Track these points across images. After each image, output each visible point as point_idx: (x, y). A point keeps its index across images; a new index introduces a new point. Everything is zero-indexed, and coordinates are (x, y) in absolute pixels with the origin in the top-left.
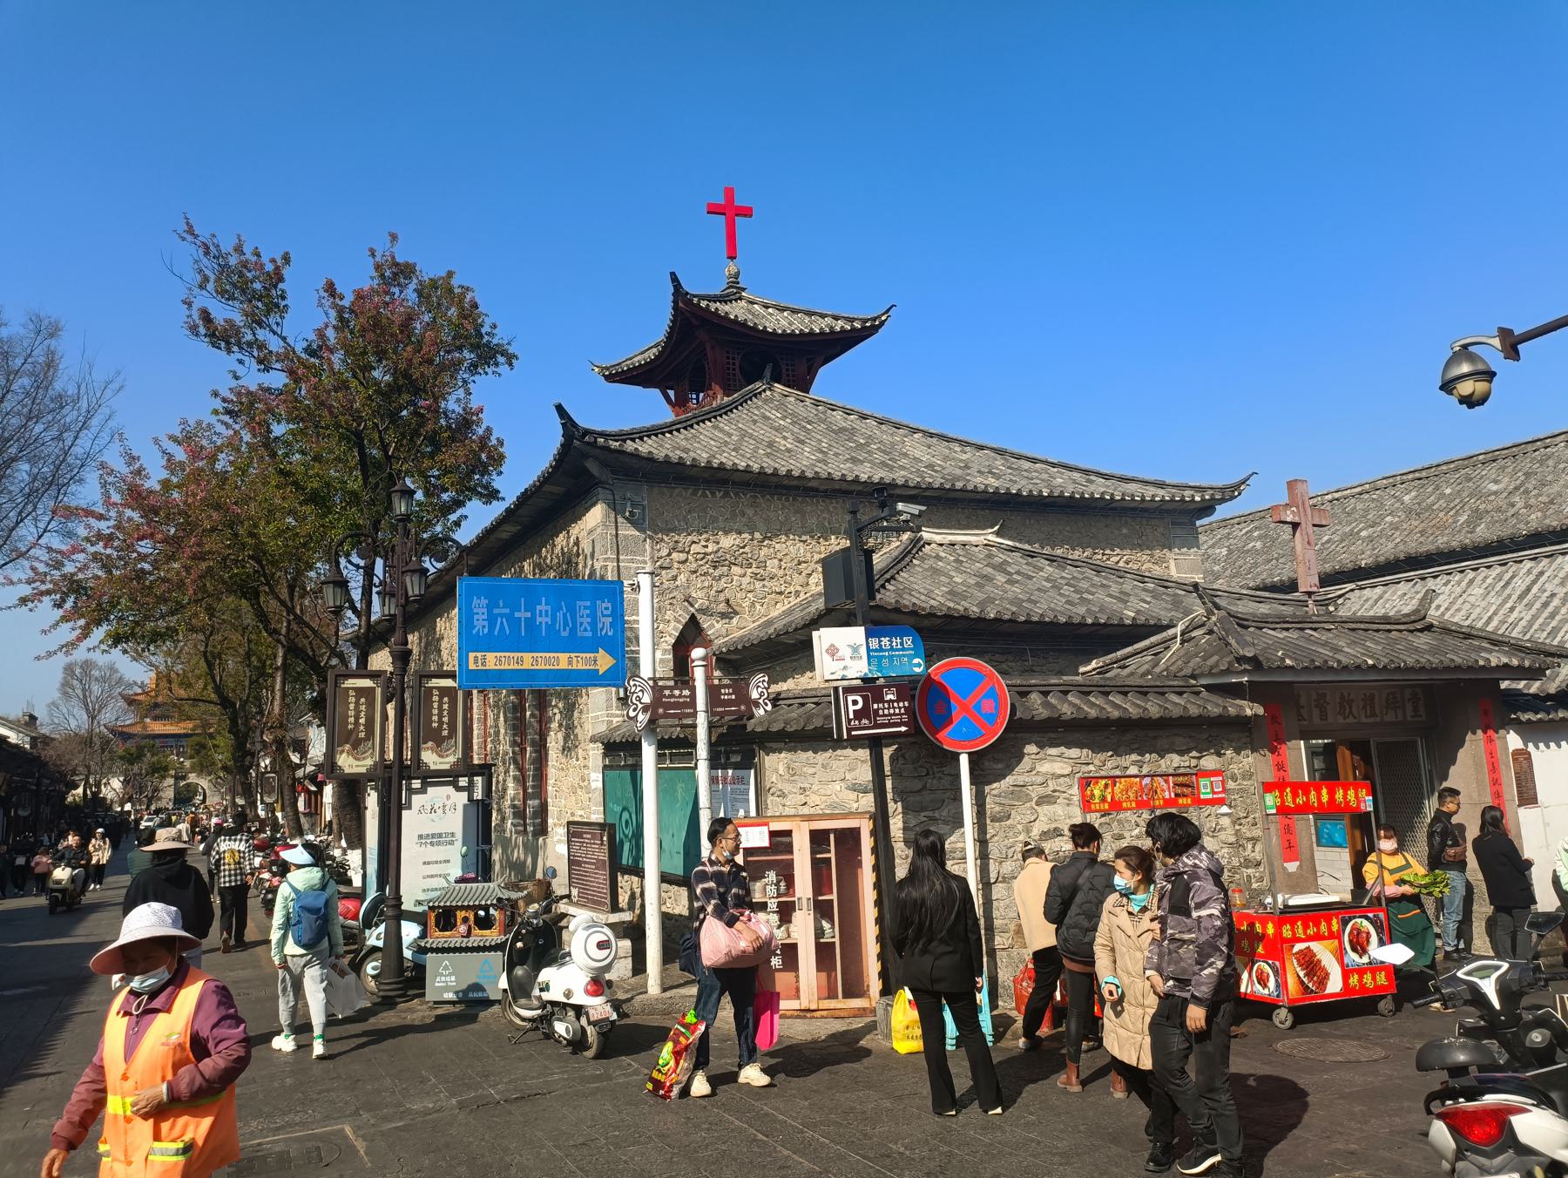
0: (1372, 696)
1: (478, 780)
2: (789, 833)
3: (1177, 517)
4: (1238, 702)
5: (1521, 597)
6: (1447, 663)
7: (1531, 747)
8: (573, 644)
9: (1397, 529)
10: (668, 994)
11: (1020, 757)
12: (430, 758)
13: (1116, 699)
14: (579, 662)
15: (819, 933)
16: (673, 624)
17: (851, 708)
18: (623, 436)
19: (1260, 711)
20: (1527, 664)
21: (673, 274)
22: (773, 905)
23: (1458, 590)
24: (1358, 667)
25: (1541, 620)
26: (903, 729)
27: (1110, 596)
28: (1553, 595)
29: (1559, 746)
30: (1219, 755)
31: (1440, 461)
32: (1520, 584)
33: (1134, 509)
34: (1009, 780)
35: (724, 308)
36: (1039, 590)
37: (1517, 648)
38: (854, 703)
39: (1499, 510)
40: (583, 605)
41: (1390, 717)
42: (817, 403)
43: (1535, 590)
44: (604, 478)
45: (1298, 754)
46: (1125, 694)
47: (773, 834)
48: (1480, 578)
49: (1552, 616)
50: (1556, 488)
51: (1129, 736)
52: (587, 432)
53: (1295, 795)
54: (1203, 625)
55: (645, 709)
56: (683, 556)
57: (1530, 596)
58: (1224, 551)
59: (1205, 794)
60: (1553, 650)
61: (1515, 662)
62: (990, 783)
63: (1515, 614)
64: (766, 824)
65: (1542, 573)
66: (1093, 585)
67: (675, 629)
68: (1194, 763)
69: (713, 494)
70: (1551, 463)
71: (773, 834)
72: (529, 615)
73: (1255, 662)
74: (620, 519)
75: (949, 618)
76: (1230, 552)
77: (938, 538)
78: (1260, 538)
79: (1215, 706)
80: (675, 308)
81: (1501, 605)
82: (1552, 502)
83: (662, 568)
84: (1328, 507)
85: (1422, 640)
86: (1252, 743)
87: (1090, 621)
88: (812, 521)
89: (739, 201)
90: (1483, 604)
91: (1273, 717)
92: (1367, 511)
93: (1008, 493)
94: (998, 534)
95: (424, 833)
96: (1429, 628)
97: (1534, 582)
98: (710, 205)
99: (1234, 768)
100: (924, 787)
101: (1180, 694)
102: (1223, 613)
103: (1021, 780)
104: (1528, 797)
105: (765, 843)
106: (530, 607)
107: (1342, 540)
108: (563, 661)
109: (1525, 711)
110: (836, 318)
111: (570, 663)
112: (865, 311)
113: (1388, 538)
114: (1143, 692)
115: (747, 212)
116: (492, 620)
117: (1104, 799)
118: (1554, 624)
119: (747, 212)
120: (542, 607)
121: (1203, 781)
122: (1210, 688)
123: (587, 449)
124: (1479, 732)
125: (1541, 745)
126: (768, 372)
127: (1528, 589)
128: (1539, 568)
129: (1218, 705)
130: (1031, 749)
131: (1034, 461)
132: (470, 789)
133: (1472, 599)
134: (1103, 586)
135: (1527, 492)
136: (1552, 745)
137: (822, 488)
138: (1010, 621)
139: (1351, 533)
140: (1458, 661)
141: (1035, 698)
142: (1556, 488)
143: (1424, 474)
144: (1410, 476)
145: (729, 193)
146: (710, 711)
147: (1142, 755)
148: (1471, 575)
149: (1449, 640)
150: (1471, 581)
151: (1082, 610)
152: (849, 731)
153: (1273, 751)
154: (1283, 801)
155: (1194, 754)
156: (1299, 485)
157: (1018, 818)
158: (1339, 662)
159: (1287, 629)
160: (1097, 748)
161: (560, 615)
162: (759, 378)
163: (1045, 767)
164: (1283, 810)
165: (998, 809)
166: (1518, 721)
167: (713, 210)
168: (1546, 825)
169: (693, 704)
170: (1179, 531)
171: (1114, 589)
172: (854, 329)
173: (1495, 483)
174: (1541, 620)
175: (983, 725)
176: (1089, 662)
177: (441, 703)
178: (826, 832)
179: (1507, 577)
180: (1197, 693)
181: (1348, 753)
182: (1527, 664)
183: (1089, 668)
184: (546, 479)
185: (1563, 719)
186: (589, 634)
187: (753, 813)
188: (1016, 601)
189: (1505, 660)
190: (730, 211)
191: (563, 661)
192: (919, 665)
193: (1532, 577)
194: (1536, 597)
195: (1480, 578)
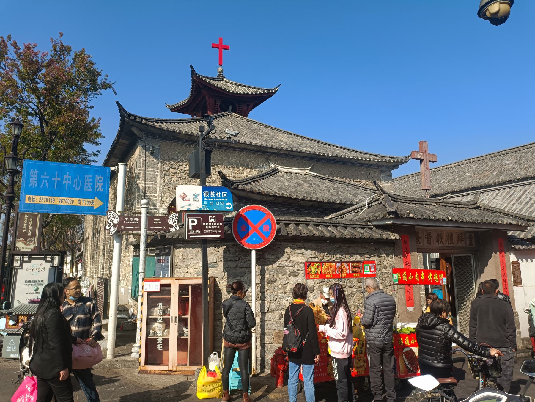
0: (452, 235)
1: (57, 258)
2: (169, 285)
3: (385, 168)
4: (389, 233)
5: (517, 200)
6: (484, 221)
7: (520, 261)
8: (81, 194)
9: (470, 177)
10: (115, 359)
11: (283, 253)
12: (21, 246)
13: (331, 229)
14: (85, 202)
15: (181, 333)
16: (168, 198)
17: (191, 224)
18: (152, 120)
19: (398, 237)
20: (519, 224)
21: (191, 65)
22: (160, 319)
23: (492, 197)
24: (444, 220)
25: (525, 209)
26: (218, 236)
27: (350, 194)
28: (531, 199)
29: (532, 261)
30: (379, 257)
31: (488, 154)
32: (517, 195)
33: (367, 164)
34: (277, 264)
35: (216, 83)
36: (320, 190)
37: (516, 217)
38: (193, 222)
39: (509, 170)
40: (88, 178)
41: (459, 245)
42: (248, 121)
43: (523, 197)
44: (141, 136)
45: (417, 259)
46: (336, 227)
47: (162, 285)
48: (501, 193)
49: (530, 207)
50: (532, 162)
51: (335, 246)
52: (130, 115)
53: (408, 275)
54: (378, 200)
55: (115, 226)
56: (175, 171)
57: (521, 200)
58: (405, 186)
59: (367, 272)
60: (530, 219)
61: (514, 223)
62: (267, 265)
63: (515, 207)
64: (159, 281)
65: (526, 191)
66: (344, 190)
67: (169, 200)
68: (366, 259)
69: (190, 146)
70: (530, 153)
71: (162, 285)
72: (59, 179)
73: (395, 213)
74: (147, 154)
75: (275, 196)
76: (407, 186)
77: (285, 170)
78: (418, 182)
79: (376, 234)
80: (193, 80)
81: (509, 203)
82: (530, 167)
83: (165, 175)
84: (444, 171)
85: (475, 212)
86: (394, 252)
87: (338, 202)
88: (232, 160)
89: (224, 43)
90: (502, 203)
91: (405, 241)
92: (459, 171)
93: (315, 154)
94: (310, 170)
95: (28, 280)
96: (478, 208)
97: (523, 194)
98: (213, 44)
99: (386, 263)
100: (237, 266)
101: (363, 228)
102: (386, 195)
103: (282, 264)
104: (518, 282)
105: (158, 290)
106: (60, 176)
107: (449, 182)
108: (75, 202)
109: (518, 244)
110: (258, 89)
111: (79, 203)
112: (269, 87)
113: (466, 181)
114: (345, 226)
115: (227, 48)
116: (39, 181)
117: (316, 273)
118: (531, 210)
119: (227, 48)
120: (67, 176)
121: (366, 266)
122: (377, 227)
123: (131, 122)
124: (498, 253)
125: (524, 260)
126: (230, 108)
127: (520, 197)
128: (525, 189)
129: (378, 233)
130: (288, 250)
131: (330, 145)
132: (52, 261)
133: (497, 201)
134: (349, 190)
135: (520, 164)
136: (529, 260)
137: (237, 147)
138: (302, 200)
139: (452, 179)
140: (490, 220)
141: (292, 226)
142: (532, 162)
143: (481, 158)
144: (476, 159)
145: (221, 40)
146: (147, 228)
147: (342, 255)
148: (497, 192)
149: (486, 213)
150: (497, 194)
151: (335, 198)
152: (189, 235)
153: (404, 256)
154: (402, 278)
155: (367, 255)
156: (424, 143)
157: (280, 282)
158: (435, 217)
159: (415, 204)
160: (320, 251)
161: (76, 181)
162: (227, 110)
163: (294, 259)
164: (401, 282)
165: (270, 277)
166: (515, 249)
167: (214, 46)
168: (525, 294)
169: (139, 224)
170: (384, 174)
171: (353, 192)
172: (264, 93)
173: (507, 161)
174: (525, 209)
175: (263, 237)
176: (328, 215)
177: (28, 221)
178: (187, 285)
179: (511, 192)
180: (371, 229)
181: (444, 262)
182: (519, 224)
183: (328, 218)
184: (119, 136)
185: (534, 249)
186: (90, 190)
187: (169, 276)
188: (309, 193)
189: (510, 221)
190: (221, 47)
191: (75, 202)
192: (229, 206)
193: (522, 192)
194: (524, 200)
195: (501, 193)
